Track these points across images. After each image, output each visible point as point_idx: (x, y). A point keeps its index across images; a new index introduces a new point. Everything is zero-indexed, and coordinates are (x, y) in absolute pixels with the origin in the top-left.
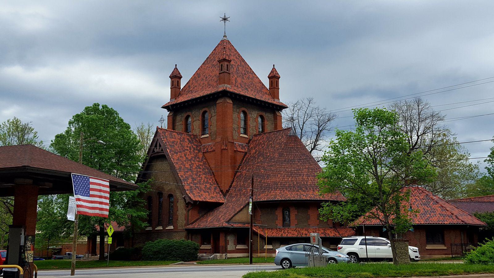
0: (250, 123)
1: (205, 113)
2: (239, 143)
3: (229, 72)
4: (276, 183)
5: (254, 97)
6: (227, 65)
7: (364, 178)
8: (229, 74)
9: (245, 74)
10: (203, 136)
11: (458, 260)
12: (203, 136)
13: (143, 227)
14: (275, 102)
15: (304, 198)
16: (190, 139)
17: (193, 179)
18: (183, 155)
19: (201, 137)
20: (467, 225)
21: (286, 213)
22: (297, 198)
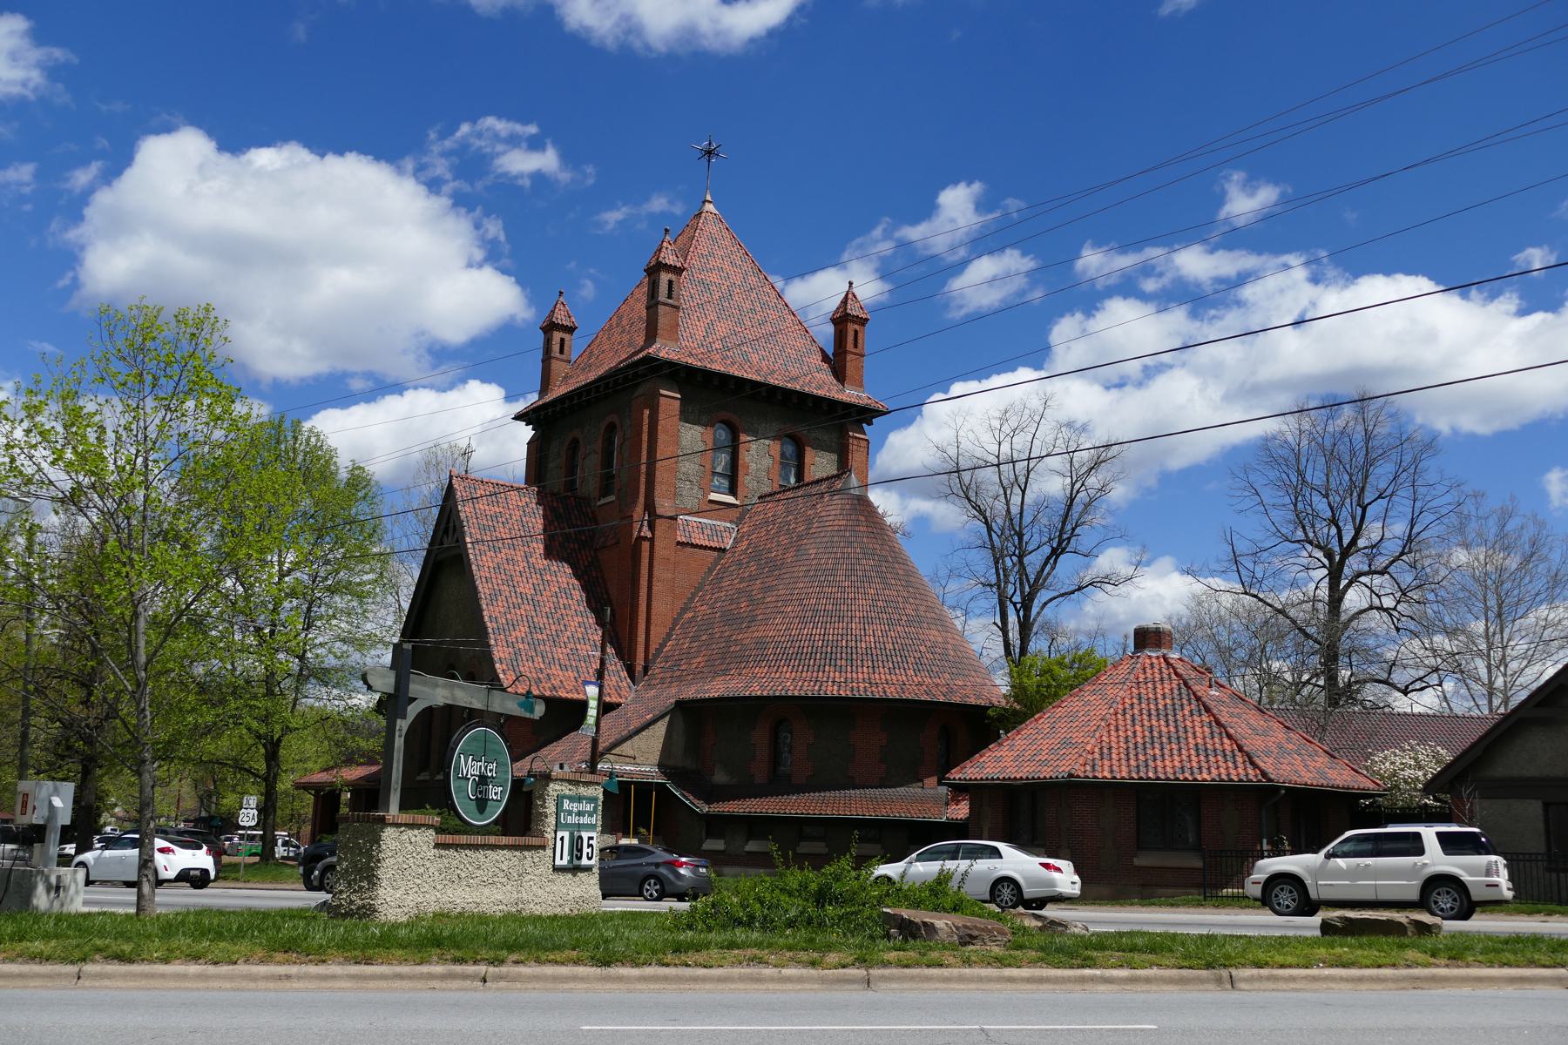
0: (747, 459)
1: (611, 428)
2: (700, 520)
3: (676, 303)
4: (761, 644)
5: (758, 379)
6: (670, 282)
7: (59, 577)
8: (677, 308)
9: (753, 311)
10: (603, 501)
11: (1172, 905)
12: (603, 501)
13: (963, 800)
14: (849, 394)
15: (832, 691)
16: (561, 510)
17: (534, 628)
18: (519, 556)
19: (599, 503)
20: (1276, 789)
21: (786, 738)
22: (806, 689)
